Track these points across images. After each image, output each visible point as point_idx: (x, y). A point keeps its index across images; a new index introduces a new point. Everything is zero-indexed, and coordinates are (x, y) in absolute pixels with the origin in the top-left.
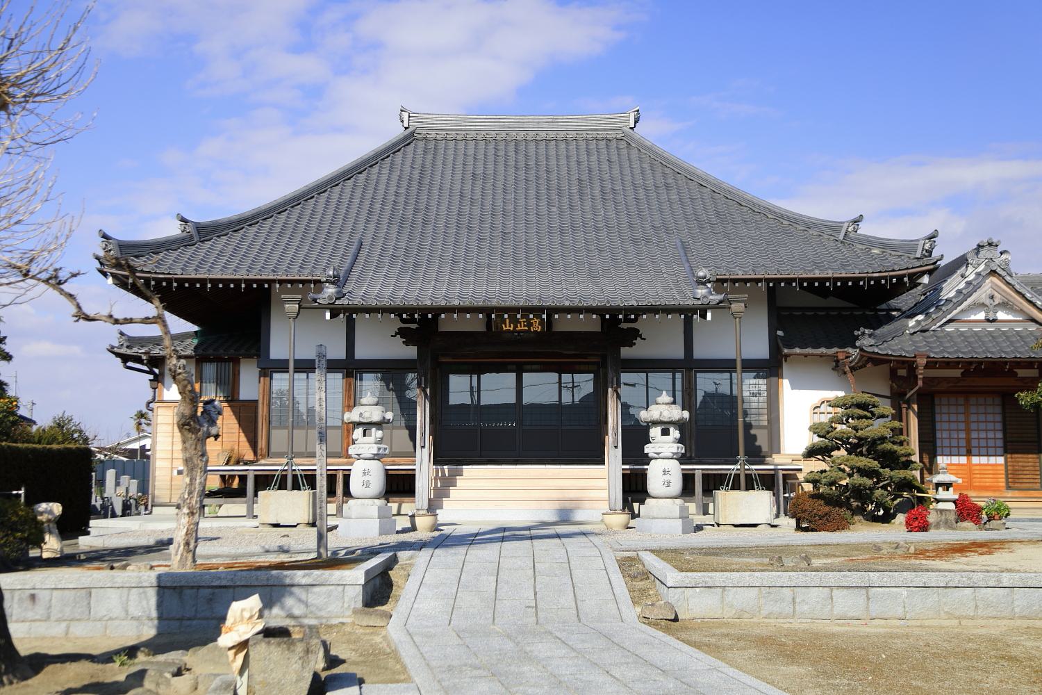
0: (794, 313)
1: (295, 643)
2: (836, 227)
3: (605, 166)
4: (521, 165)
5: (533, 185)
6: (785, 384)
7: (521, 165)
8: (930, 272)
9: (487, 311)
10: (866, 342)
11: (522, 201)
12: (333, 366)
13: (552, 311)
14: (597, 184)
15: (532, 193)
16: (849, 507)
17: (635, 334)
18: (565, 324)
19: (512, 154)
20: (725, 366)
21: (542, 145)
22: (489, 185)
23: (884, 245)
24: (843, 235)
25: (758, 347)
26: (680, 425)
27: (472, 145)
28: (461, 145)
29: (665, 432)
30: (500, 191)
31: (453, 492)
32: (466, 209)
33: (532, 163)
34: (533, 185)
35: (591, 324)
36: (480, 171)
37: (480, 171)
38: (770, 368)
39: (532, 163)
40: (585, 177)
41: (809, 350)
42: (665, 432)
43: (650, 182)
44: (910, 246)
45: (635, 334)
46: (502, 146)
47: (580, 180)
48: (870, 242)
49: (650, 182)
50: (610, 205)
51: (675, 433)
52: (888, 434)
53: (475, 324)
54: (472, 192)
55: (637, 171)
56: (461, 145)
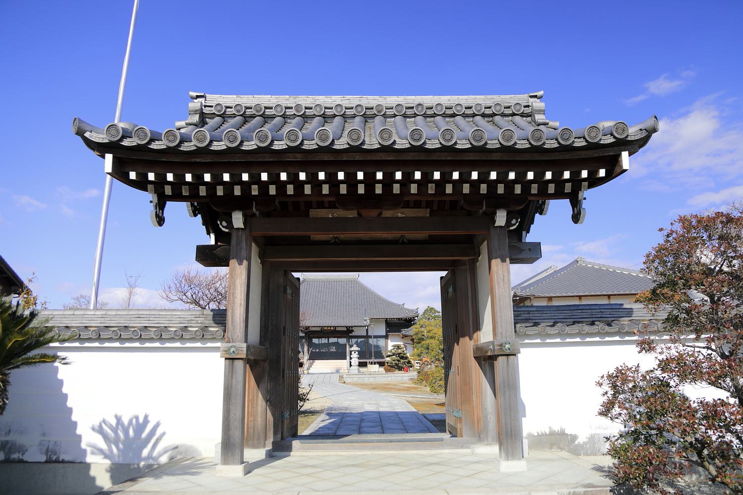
0: (25, 345)
1: (659, 366)
2: (399, 305)
3: (350, 288)
4: (330, 288)
5: (332, 293)
6: (389, 341)
7: (330, 288)
8: (417, 317)
9: (346, 327)
10: (403, 332)
11: (329, 298)
12: (371, 337)
13: (336, 327)
14: (348, 293)
15: (332, 295)
16: (395, 368)
17: (353, 331)
18: (338, 329)
19: (328, 285)
20: (376, 337)
21: (335, 283)
22: (322, 293)
23: (408, 310)
24: (401, 307)
25: (384, 334)
26: (358, 351)
27: (318, 282)
28: (340, 283)
29: (355, 353)
30: (325, 295)
31: (311, 368)
32: (316, 300)
33: (333, 288)
34: (332, 293)
35: (345, 329)
36: (320, 290)
37: (320, 290)
38: (386, 337)
39: (333, 288)
40: (345, 291)
41: (393, 333)
42: (355, 353)
43: (360, 293)
44: (413, 311)
45: (353, 331)
46: (326, 283)
47: (344, 292)
48: (406, 309)
49: (360, 293)
50: (350, 299)
51: (357, 353)
52: (402, 352)
53: (319, 329)
54: (318, 296)
55: (358, 290)
56: (340, 283)
